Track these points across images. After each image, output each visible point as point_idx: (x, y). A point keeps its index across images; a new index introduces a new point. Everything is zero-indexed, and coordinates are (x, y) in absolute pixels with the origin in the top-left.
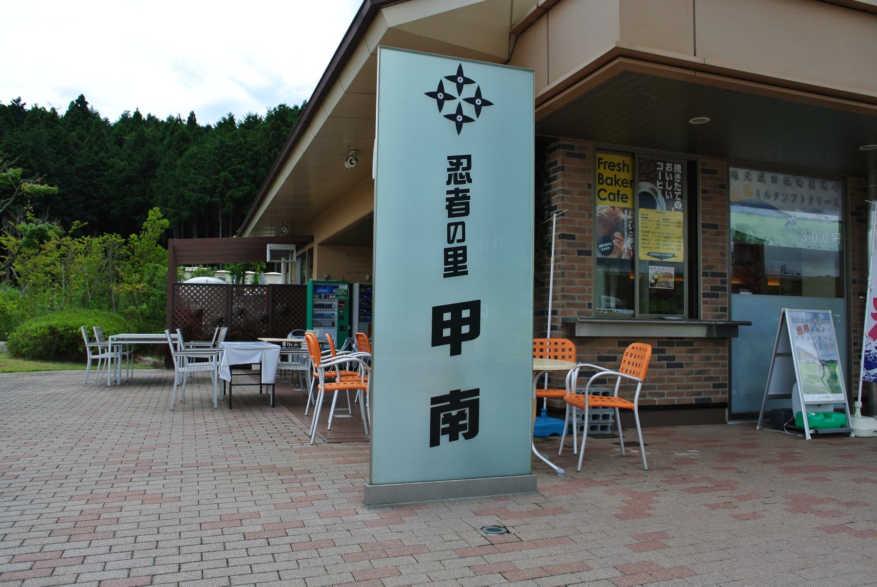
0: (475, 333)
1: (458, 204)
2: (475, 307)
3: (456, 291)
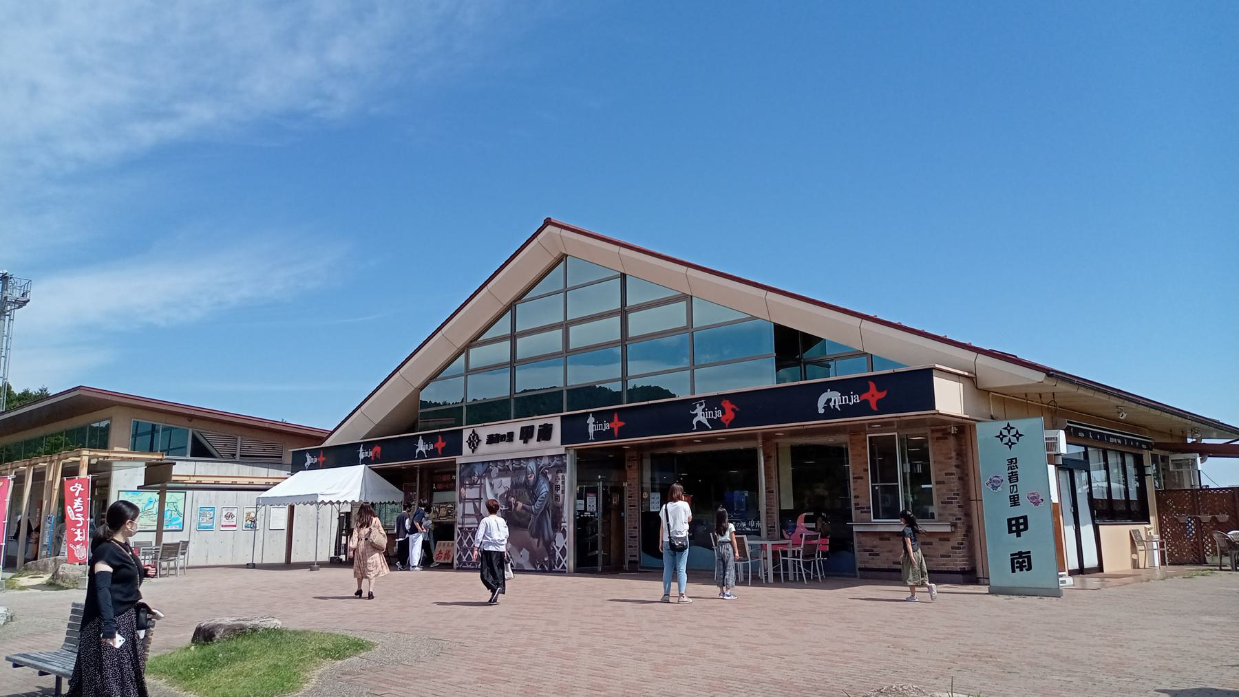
0: (1026, 528)
1: (1013, 477)
2: (1025, 518)
3: (1017, 512)
